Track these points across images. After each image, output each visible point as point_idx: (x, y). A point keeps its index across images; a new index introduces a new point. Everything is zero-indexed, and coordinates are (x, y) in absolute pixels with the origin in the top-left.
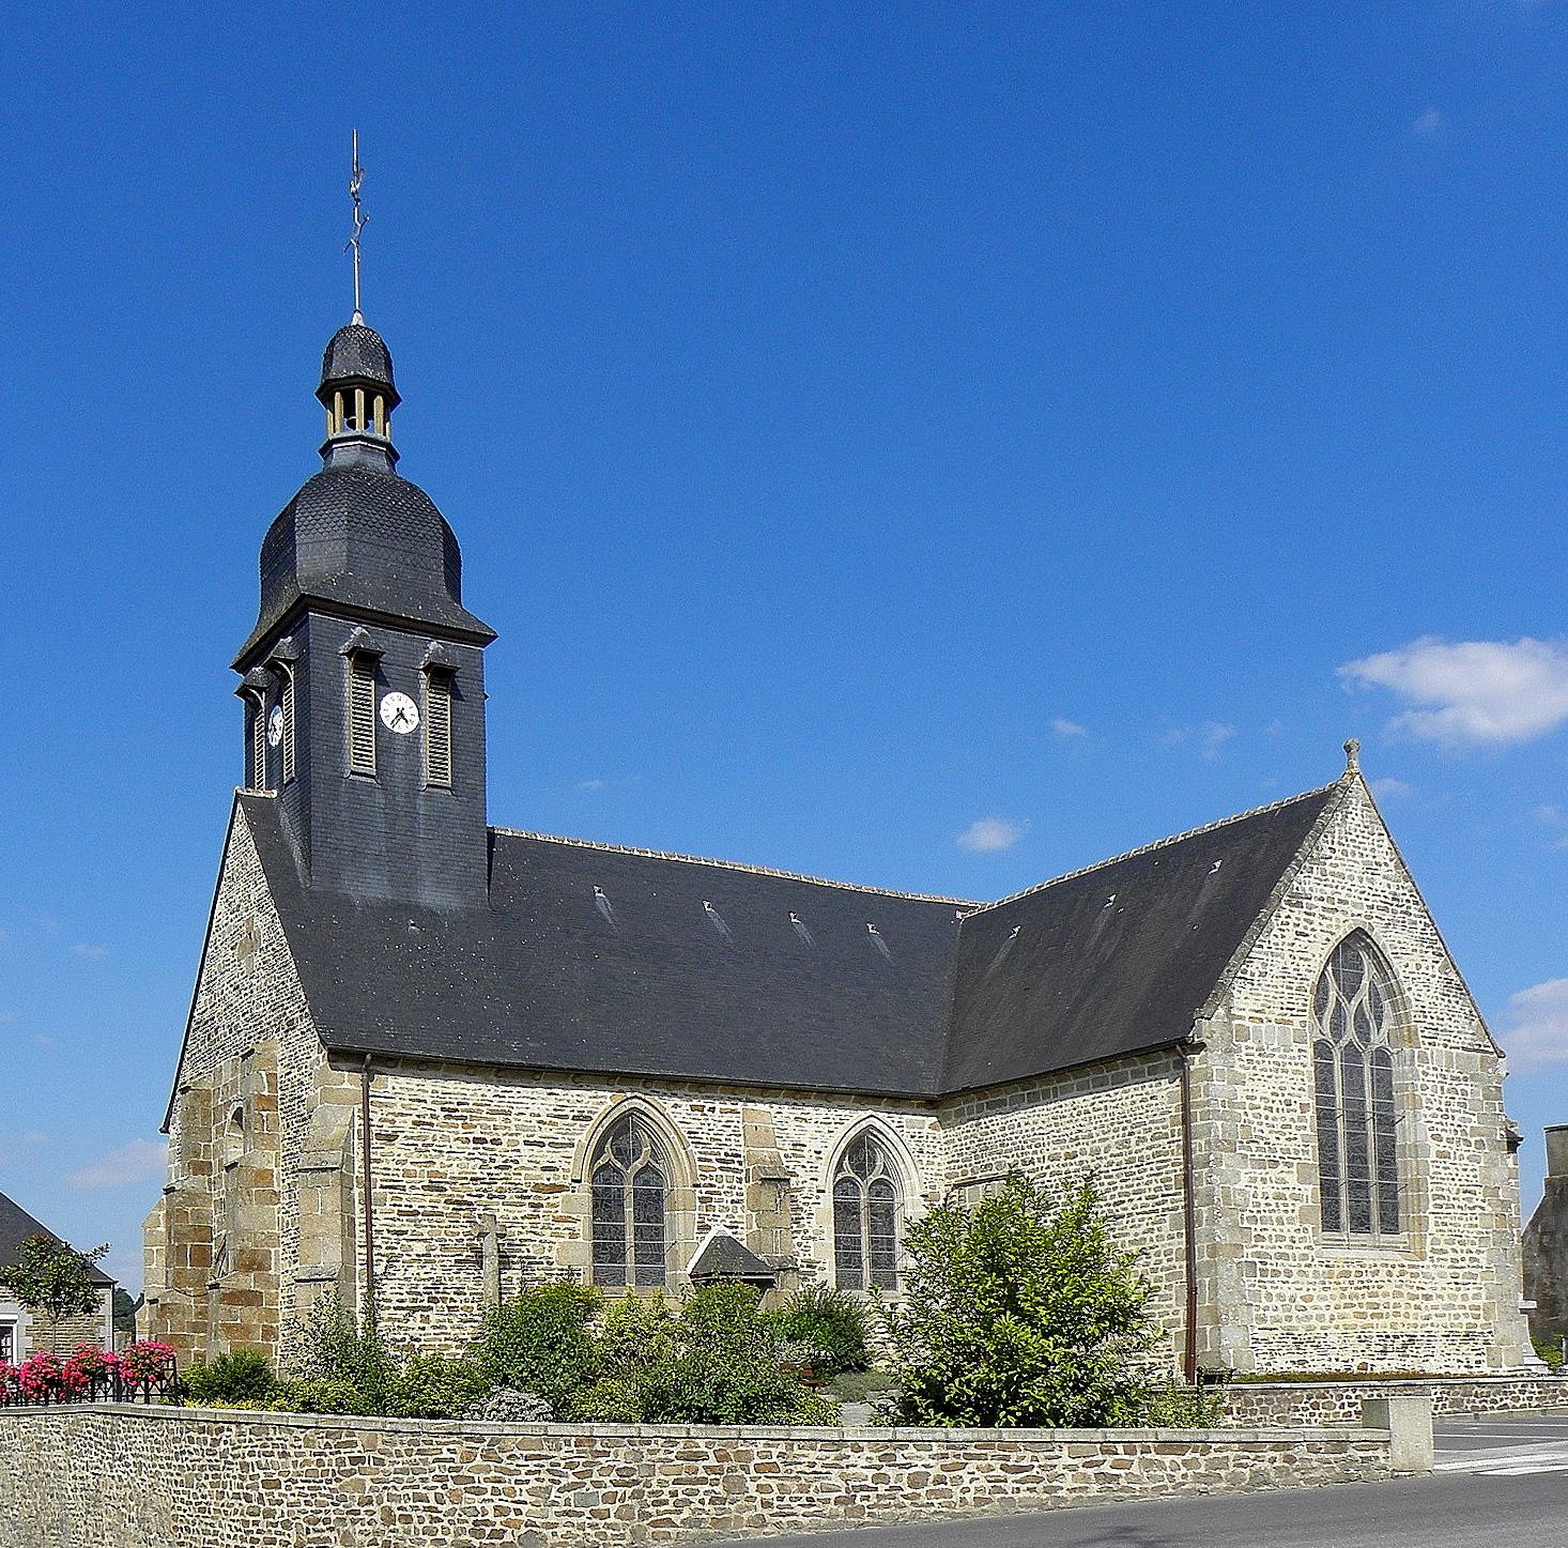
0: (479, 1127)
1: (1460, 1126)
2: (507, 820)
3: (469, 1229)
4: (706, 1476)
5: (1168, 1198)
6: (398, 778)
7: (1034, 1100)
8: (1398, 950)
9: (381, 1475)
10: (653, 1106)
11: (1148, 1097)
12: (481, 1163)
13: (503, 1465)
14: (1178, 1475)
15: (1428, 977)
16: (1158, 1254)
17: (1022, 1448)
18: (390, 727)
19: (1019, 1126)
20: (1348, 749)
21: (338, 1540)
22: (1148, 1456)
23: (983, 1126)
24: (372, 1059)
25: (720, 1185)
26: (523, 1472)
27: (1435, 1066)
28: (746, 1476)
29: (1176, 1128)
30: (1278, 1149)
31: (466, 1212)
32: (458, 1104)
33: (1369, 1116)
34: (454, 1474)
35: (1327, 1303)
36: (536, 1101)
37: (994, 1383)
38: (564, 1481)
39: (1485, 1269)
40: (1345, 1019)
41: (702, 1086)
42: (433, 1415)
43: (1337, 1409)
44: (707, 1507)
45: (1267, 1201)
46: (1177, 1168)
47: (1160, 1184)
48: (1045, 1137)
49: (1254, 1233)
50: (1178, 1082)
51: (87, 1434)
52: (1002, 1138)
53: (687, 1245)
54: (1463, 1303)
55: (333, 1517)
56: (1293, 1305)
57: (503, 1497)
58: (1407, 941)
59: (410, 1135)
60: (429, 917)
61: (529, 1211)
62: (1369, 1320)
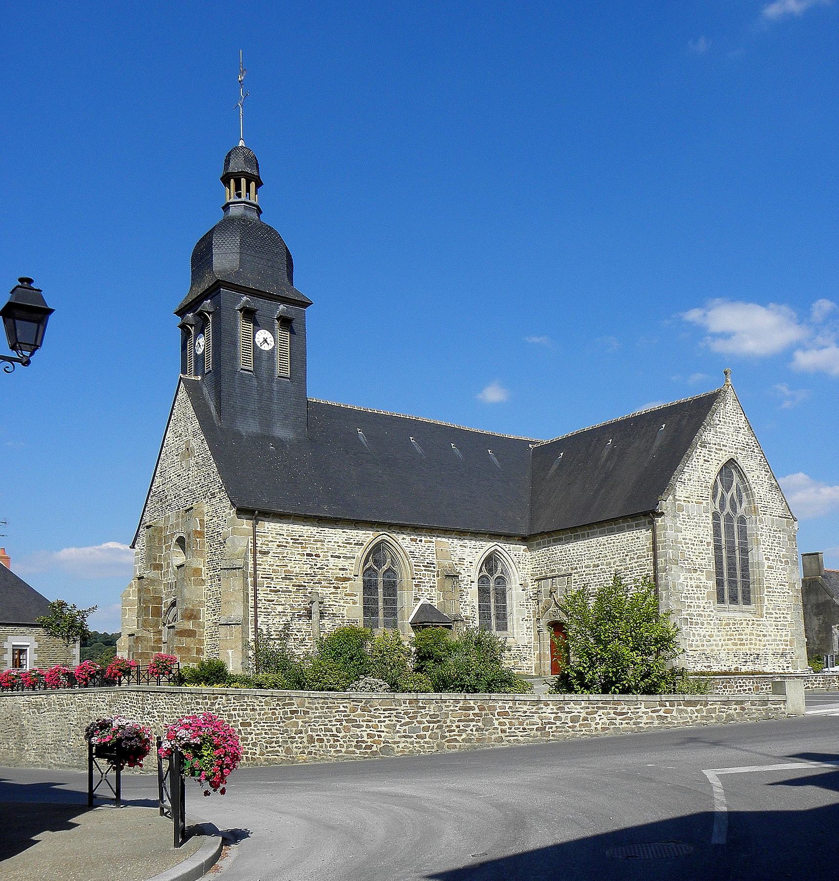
0: (309, 548)
1: (777, 553)
2: (313, 396)
3: (304, 599)
4: (474, 718)
6: (264, 374)
7: (577, 538)
9: (307, 719)
10: (393, 539)
11: (635, 538)
12: (310, 566)
13: (372, 713)
14: (694, 716)
15: (763, 482)
17: (623, 704)
18: (259, 345)
19: (569, 551)
20: (726, 373)
21: (283, 751)
22: (680, 707)
23: (551, 550)
24: (258, 514)
25: (425, 578)
26: (382, 717)
27: (766, 524)
28: (493, 718)
29: (650, 553)
30: (697, 564)
31: (302, 590)
32: (299, 536)
33: (737, 548)
34: (346, 718)
35: (720, 638)
36: (336, 536)
37: (610, 673)
38: (403, 721)
39: (790, 622)
40: (726, 501)
41: (416, 529)
42: (330, 690)
43: (735, 689)
44: (474, 733)
48: (583, 556)
49: (687, 604)
50: (650, 531)
51: (124, 702)
52: (560, 557)
53: (409, 610)
54: (781, 639)
55: (281, 740)
56: (705, 639)
57: (371, 729)
58: (753, 465)
59: (276, 552)
60: (280, 443)
61: (333, 590)
62: (739, 647)
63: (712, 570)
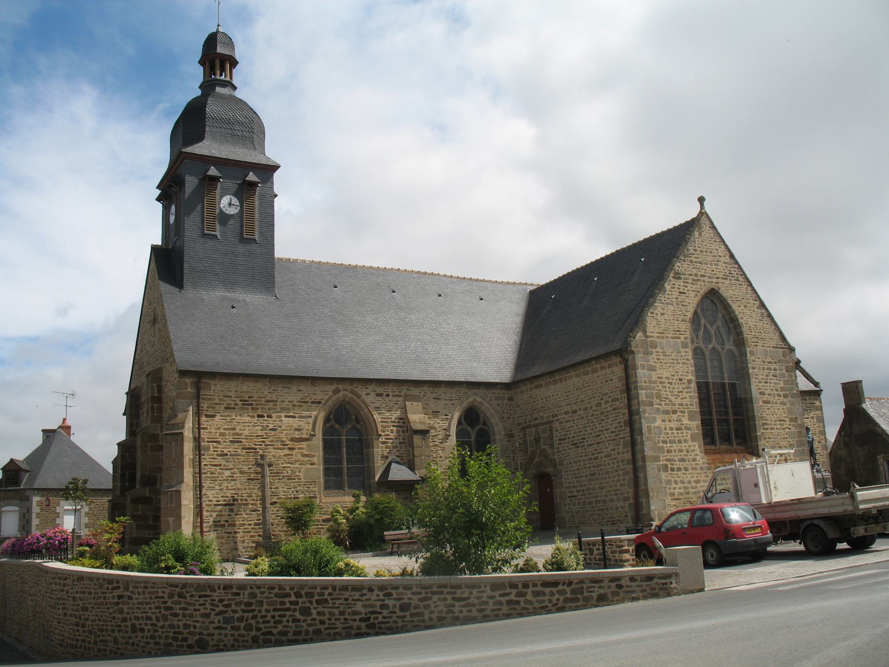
5: (622, 432)
8: (734, 299)
12: (262, 428)
14: (554, 599)
16: (618, 462)
22: (536, 589)
27: (759, 356)
38: (217, 609)
44: (291, 624)
45: (673, 431)
46: (625, 416)
47: (617, 425)
63: (695, 410)
